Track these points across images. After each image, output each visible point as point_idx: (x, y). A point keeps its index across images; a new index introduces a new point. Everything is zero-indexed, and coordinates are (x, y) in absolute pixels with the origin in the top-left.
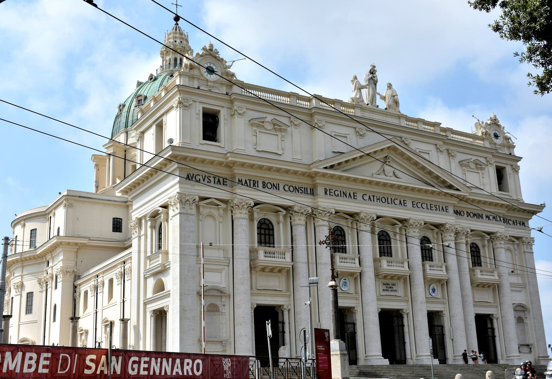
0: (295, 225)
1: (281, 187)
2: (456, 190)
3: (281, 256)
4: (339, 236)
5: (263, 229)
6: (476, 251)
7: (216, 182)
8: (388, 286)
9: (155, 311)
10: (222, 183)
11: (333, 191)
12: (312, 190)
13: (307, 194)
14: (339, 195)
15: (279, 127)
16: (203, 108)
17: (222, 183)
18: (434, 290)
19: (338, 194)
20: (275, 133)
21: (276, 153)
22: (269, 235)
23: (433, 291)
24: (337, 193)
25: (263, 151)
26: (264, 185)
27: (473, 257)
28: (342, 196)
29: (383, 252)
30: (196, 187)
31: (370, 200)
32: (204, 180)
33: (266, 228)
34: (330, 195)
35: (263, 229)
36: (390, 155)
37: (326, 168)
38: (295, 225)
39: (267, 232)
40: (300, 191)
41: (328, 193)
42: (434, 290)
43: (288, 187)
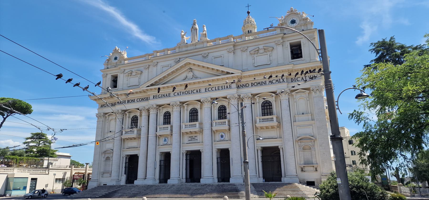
0: (282, 100)
1: (136, 101)
2: (231, 74)
8: (192, 138)
9: (264, 150)
11: (158, 96)
12: (265, 82)
14: (161, 97)
15: (267, 50)
18: (222, 136)
19: (160, 97)
20: (266, 54)
21: (267, 64)
22: (270, 109)
23: (221, 137)
24: (159, 97)
25: (258, 66)
28: (162, 97)
30: (104, 110)
31: (227, 88)
33: (195, 112)
35: (221, 110)
37: (148, 86)
38: (282, 100)
39: (268, 107)
40: (144, 100)
41: (155, 97)
42: (222, 136)
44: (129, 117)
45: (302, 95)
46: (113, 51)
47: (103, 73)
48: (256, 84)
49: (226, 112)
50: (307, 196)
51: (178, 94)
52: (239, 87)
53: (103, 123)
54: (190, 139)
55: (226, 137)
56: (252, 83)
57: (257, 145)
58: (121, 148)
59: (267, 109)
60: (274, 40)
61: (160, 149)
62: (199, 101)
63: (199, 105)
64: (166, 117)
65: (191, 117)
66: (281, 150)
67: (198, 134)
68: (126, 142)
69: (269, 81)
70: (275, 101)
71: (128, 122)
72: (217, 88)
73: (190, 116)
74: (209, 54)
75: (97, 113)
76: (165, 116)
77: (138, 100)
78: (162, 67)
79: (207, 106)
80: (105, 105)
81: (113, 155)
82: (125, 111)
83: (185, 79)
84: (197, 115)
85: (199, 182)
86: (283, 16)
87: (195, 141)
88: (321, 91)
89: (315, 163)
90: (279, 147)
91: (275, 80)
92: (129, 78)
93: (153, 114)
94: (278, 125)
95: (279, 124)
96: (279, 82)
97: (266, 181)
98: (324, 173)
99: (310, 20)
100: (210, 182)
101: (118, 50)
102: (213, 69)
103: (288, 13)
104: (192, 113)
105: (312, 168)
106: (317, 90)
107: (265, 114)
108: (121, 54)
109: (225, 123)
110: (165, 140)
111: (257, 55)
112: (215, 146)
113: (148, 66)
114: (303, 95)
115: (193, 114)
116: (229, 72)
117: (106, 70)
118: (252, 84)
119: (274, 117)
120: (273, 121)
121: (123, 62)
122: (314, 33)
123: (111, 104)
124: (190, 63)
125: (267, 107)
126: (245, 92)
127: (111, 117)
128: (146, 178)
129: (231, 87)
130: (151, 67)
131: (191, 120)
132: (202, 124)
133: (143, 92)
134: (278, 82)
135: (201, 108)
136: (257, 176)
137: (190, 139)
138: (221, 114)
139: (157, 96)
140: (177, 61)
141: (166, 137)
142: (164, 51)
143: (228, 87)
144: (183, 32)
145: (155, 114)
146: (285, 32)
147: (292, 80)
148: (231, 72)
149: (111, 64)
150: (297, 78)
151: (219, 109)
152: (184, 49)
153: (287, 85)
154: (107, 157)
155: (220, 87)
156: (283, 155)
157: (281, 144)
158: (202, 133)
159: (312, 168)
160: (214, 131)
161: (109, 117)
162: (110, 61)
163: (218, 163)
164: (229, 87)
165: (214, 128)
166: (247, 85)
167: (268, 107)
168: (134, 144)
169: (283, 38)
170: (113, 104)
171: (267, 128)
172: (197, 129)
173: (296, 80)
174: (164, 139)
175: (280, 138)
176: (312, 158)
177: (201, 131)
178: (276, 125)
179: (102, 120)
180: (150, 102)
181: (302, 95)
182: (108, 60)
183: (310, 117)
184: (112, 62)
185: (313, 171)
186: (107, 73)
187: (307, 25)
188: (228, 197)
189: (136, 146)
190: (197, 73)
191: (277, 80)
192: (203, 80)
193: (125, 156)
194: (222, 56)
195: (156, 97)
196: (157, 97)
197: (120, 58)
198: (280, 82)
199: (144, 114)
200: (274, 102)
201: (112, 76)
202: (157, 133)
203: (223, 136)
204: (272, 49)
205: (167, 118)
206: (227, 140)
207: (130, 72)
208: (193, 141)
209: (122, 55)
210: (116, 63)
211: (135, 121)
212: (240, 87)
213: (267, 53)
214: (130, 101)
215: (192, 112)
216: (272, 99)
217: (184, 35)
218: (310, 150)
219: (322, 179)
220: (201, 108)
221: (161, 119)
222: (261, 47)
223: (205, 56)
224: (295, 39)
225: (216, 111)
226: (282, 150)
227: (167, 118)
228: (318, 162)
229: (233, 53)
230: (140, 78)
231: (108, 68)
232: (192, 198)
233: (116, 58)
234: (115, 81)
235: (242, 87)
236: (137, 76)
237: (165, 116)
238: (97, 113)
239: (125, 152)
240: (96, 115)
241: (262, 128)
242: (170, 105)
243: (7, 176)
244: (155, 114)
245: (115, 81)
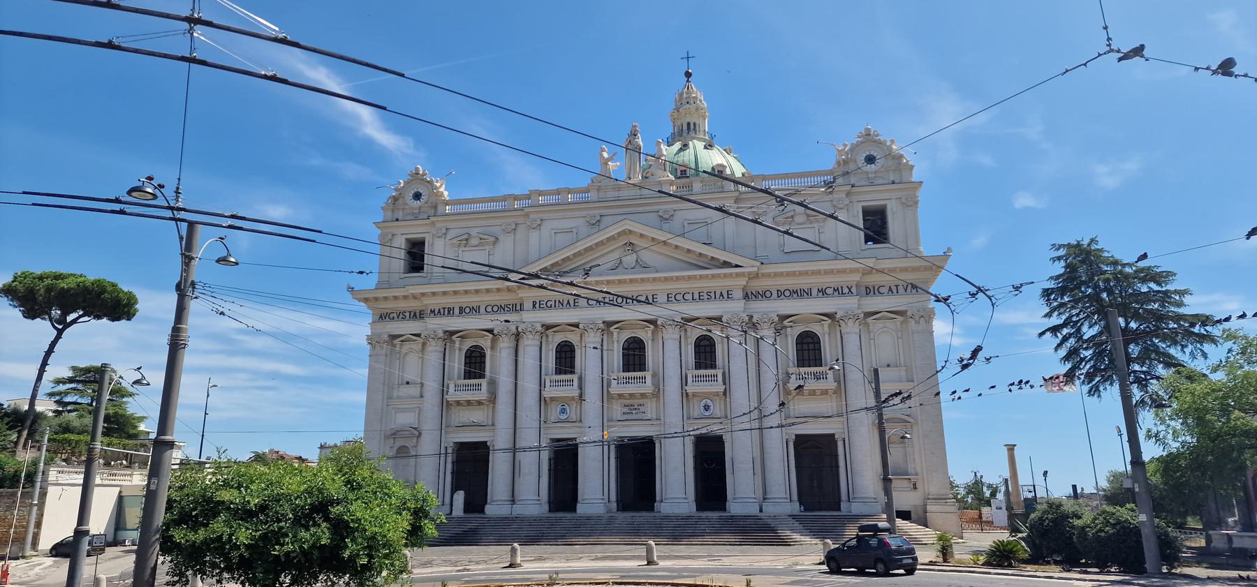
0: (848, 333)
1: (482, 310)
3: (702, 379)
4: (707, 348)
5: (806, 343)
6: (814, 343)
7: (412, 316)
9: (462, 447)
10: (418, 317)
13: (516, 310)
16: (863, 207)
17: (418, 317)
20: (811, 226)
23: (705, 409)
24: (549, 304)
26: (462, 310)
27: (558, 360)
29: (807, 358)
30: (389, 326)
32: (398, 317)
34: (540, 307)
35: (806, 343)
38: (848, 333)
39: (811, 346)
40: (506, 309)
41: (537, 306)
43: (491, 307)
44: (460, 349)
45: (413, 347)
46: (410, 175)
47: (380, 232)
50: (921, 541)
51: (890, 289)
53: (386, 359)
54: (628, 411)
55: (717, 409)
56: (778, 291)
57: (446, 438)
58: (444, 426)
59: (705, 352)
60: (498, 222)
61: (549, 431)
62: (490, 331)
63: (489, 341)
64: (563, 354)
66: (840, 444)
67: (649, 400)
68: (455, 410)
70: (653, 340)
71: (457, 363)
72: (696, 296)
74: (603, 218)
77: (489, 309)
78: (555, 233)
79: (593, 338)
80: (392, 315)
81: (417, 442)
82: (452, 333)
83: (617, 267)
84: (573, 358)
85: (482, 511)
86: (847, 143)
87: (640, 416)
88: (929, 320)
89: (913, 472)
90: (836, 437)
92: (460, 252)
93: (534, 345)
94: (654, 391)
95: (657, 390)
96: (840, 292)
97: (806, 510)
98: (933, 493)
99: (908, 161)
100: (684, 512)
101: (424, 174)
102: (689, 251)
103: (859, 137)
105: (906, 482)
106: (922, 317)
107: (634, 367)
108: (434, 187)
109: (479, 388)
110: (563, 411)
111: (465, 249)
114: (889, 324)
115: (805, 347)
116: (730, 263)
117: (390, 224)
119: (648, 375)
120: (826, 378)
121: (440, 208)
122: (915, 191)
124: (630, 231)
125: (705, 349)
126: (761, 308)
127: (409, 346)
129: (576, 304)
130: (521, 231)
131: (468, 375)
133: (411, 297)
134: (839, 294)
135: (493, 348)
136: (603, 499)
137: (626, 410)
139: (542, 302)
140: (594, 222)
141: (564, 402)
142: (558, 192)
143: (891, 290)
144: (605, 151)
145: (440, 352)
146: (853, 180)
147: (868, 291)
148: (734, 262)
149: (403, 209)
152: (611, 194)
153: (859, 300)
154: (401, 445)
155: (705, 294)
156: (843, 454)
157: (842, 431)
159: (906, 484)
160: (545, 400)
161: (401, 345)
162: (401, 201)
163: (550, 470)
164: (725, 296)
165: (546, 394)
166: (768, 294)
167: (811, 346)
168: (477, 415)
169: (848, 194)
170: (415, 313)
171: (469, 403)
172: (648, 387)
173: (876, 291)
174: (559, 407)
175: (657, 419)
176: (906, 461)
177: (657, 393)
178: (834, 388)
179: (384, 351)
180: (523, 316)
181: (413, 347)
182: (394, 197)
183: (903, 373)
184: (407, 204)
185: (908, 489)
186: (395, 231)
187: (900, 170)
188: (653, 543)
189: (483, 422)
190: (646, 256)
192: (678, 275)
193: (452, 445)
196: (541, 306)
197: (429, 196)
198: (842, 294)
199: (505, 344)
200: (650, 342)
201: (407, 240)
203: (709, 407)
204: (493, 239)
206: (575, 420)
207: (465, 237)
208: (634, 414)
209: (436, 188)
210: (420, 207)
211: (475, 363)
213: (485, 248)
216: (645, 335)
217: (608, 160)
218: (903, 445)
219: (928, 506)
220: (493, 348)
221: (616, 357)
222: (474, 232)
223: (667, 216)
224: (874, 200)
225: (689, 347)
226: (842, 442)
228: (919, 470)
231: (397, 220)
232: (633, 546)
233: (417, 196)
234: (416, 257)
236: (482, 248)
237: (799, 343)
239: (453, 435)
241: (458, 403)
242: (580, 327)
243: (120, 492)
244: (440, 352)
245: (416, 257)
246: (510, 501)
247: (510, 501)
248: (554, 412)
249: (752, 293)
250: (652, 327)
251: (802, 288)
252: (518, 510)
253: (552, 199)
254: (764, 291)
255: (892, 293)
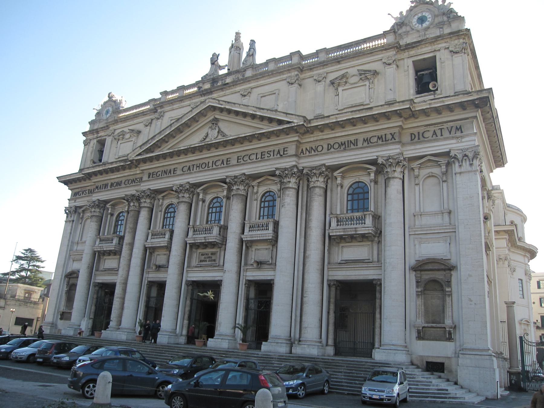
8: (207, 256)
11: (242, 158)
36: (217, 117)
40: (136, 181)
41: (151, 176)
48: (336, 146)
49: (274, 205)
52: (303, 152)
56: (411, 134)
59: (358, 200)
65: (350, 203)
69: (364, 139)
73: (348, 201)
75: (68, 206)
76: (263, 202)
80: (80, 193)
91: (254, 154)
96: (384, 139)
104: (352, 194)
112: (245, 275)
113: (150, 121)
118: (330, 146)
123: (89, 190)
128: (119, 329)
132: (378, 219)
134: (383, 141)
138: (356, 203)
139: (154, 173)
143: (436, 134)
150: (424, 132)
151: (351, 191)
158: (379, 242)
166: (320, 149)
167: (361, 196)
189: (369, 259)
191: (458, 127)
194: (277, 92)
195: (153, 175)
198: (386, 141)
202: (243, 237)
205: (170, 217)
212: (305, 152)
213: (365, 83)
214: (115, 185)
215: (214, 206)
227: (216, 212)
229: (394, 66)
230: (136, 143)
235: (309, 152)
238: (68, 206)
240: (65, 211)
246: (286, 340)
247: (286, 340)
248: (255, 254)
249: (306, 149)
250: (374, 168)
251: (349, 140)
252: (298, 350)
253: (176, 95)
254: (317, 146)
255: (437, 136)
